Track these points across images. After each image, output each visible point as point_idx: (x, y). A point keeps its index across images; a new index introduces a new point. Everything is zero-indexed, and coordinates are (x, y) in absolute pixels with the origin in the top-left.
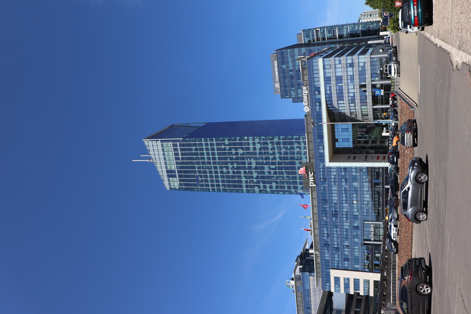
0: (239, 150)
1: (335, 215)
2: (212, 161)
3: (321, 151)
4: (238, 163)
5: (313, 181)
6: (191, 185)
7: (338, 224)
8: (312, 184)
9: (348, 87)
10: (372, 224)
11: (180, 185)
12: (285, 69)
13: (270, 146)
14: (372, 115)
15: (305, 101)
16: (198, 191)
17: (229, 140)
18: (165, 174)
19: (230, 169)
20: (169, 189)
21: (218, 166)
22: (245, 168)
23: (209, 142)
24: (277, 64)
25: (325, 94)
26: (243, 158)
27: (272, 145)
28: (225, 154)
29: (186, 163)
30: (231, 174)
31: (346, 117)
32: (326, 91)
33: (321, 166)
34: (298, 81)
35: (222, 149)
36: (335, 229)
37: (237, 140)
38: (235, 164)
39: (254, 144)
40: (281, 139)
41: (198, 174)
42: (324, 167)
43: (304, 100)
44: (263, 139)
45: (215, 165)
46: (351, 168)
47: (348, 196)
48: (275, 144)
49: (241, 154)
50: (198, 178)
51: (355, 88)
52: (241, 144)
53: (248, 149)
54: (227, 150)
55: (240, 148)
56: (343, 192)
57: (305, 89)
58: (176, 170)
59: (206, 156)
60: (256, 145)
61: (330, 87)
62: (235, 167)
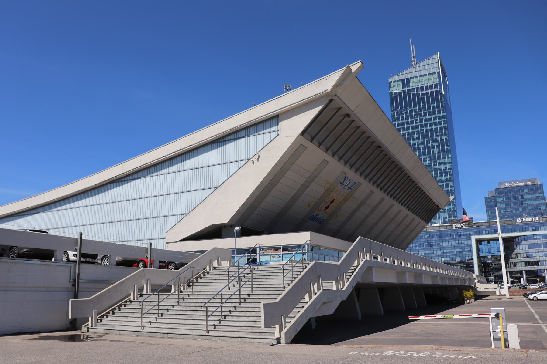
0: (438, 149)
1: (430, 245)
2: (424, 123)
3: (484, 232)
4: (424, 148)
5: (458, 227)
6: (396, 103)
7: (422, 248)
8: (455, 226)
9: (541, 252)
11: (396, 93)
12: (524, 192)
13: (444, 178)
14: (516, 270)
15: (526, 219)
16: (392, 111)
17: (446, 139)
18: (405, 77)
19: (418, 141)
20: (389, 81)
21: (419, 129)
23: (442, 120)
24: (528, 184)
26: (429, 153)
27: (445, 180)
28: (432, 136)
29: (418, 98)
30: (412, 142)
31: (512, 250)
32: (536, 235)
33: (471, 233)
34: (513, 204)
35: (436, 133)
36: (417, 245)
37: (447, 148)
38: (423, 146)
39: (445, 163)
40: (451, 188)
41: (409, 110)
42: (470, 235)
44: (450, 171)
45: (420, 127)
46: (472, 255)
47: (448, 254)
48: (446, 183)
49: (433, 151)
50: (404, 110)
51: (540, 257)
52: (443, 151)
53: (439, 158)
54: (436, 138)
55: (439, 150)
56: (451, 250)
57: (536, 219)
58: (410, 88)
59: (428, 117)
60: (444, 165)
61: (539, 238)
62: (420, 146)
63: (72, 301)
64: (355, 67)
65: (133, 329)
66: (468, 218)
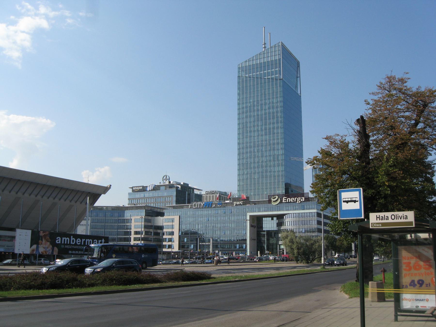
5: (237, 204)
10: (210, 244)
22: (274, 128)
25: (304, 213)
43: (299, 198)
63: (413, 225)
64: (430, 189)
65: (257, 266)
66: (245, 197)
